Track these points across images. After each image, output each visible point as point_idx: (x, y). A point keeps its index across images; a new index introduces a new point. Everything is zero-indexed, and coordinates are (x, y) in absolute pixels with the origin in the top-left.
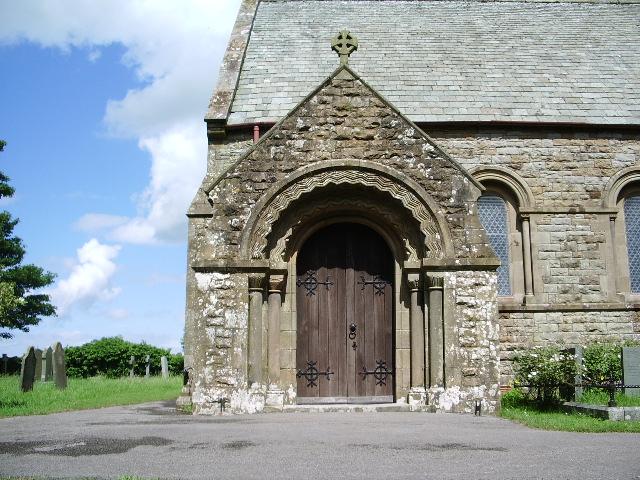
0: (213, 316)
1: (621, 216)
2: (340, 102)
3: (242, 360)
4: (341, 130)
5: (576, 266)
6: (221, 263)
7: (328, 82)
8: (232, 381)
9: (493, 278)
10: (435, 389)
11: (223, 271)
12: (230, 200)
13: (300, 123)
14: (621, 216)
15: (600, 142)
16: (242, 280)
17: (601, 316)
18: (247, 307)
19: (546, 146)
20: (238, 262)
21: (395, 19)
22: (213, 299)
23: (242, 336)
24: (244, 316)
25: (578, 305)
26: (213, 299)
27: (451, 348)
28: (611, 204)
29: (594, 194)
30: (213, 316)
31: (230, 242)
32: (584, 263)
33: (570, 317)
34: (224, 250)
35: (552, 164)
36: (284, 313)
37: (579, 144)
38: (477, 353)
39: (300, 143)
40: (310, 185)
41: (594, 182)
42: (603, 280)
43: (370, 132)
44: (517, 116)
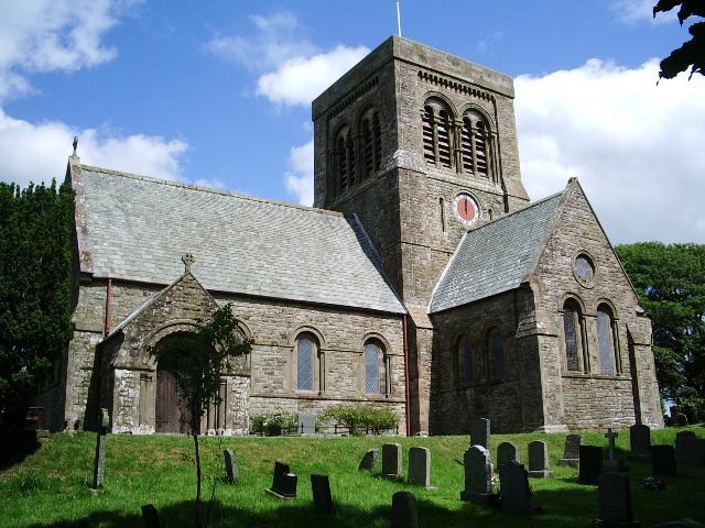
0: (123, 391)
1: (296, 349)
2: (187, 290)
3: (136, 413)
4: (187, 305)
5: (272, 374)
6: (129, 365)
7: (181, 280)
8: (132, 423)
9: (248, 381)
10: (221, 430)
11: (129, 369)
12: (133, 334)
13: (168, 299)
14: (296, 349)
15: (289, 308)
16: (138, 374)
17: (282, 401)
18: (593, 380)
19: (264, 308)
20: (137, 365)
21: (172, 202)
22: (124, 383)
23: (136, 403)
24: (138, 392)
25: (272, 395)
26: (124, 383)
27: (229, 411)
28: (293, 342)
29: (284, 336)
30: (123, 391)
31: (132, 355)
32: (276, 372)
33: (267, 400)
34: (130, 359)
35: (265, 318)
36: (152, 387)
37: (278, 309)
38: (240, 414)
39: (167, 309)
40: (170, 330)
41: (283, 329)
42: (285, 382)
43: (199, 308)
44: (249, 291)
